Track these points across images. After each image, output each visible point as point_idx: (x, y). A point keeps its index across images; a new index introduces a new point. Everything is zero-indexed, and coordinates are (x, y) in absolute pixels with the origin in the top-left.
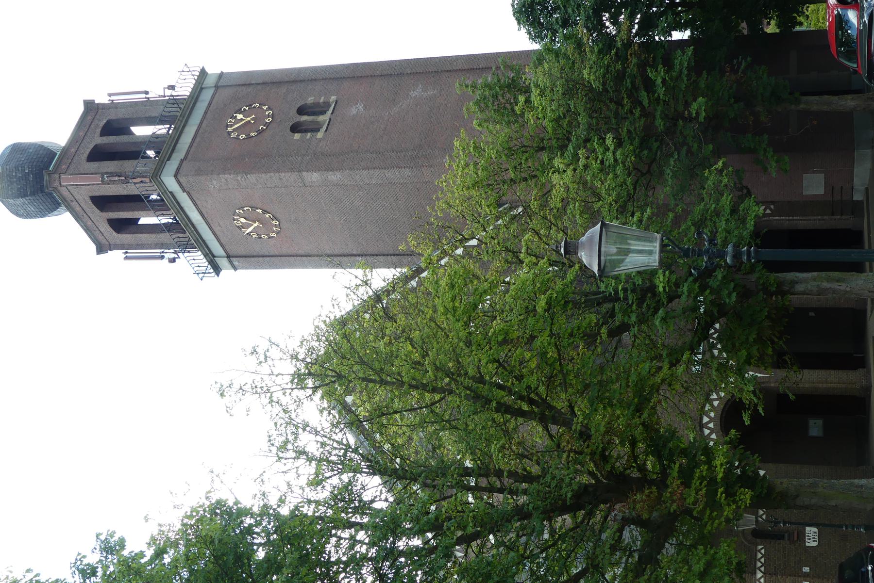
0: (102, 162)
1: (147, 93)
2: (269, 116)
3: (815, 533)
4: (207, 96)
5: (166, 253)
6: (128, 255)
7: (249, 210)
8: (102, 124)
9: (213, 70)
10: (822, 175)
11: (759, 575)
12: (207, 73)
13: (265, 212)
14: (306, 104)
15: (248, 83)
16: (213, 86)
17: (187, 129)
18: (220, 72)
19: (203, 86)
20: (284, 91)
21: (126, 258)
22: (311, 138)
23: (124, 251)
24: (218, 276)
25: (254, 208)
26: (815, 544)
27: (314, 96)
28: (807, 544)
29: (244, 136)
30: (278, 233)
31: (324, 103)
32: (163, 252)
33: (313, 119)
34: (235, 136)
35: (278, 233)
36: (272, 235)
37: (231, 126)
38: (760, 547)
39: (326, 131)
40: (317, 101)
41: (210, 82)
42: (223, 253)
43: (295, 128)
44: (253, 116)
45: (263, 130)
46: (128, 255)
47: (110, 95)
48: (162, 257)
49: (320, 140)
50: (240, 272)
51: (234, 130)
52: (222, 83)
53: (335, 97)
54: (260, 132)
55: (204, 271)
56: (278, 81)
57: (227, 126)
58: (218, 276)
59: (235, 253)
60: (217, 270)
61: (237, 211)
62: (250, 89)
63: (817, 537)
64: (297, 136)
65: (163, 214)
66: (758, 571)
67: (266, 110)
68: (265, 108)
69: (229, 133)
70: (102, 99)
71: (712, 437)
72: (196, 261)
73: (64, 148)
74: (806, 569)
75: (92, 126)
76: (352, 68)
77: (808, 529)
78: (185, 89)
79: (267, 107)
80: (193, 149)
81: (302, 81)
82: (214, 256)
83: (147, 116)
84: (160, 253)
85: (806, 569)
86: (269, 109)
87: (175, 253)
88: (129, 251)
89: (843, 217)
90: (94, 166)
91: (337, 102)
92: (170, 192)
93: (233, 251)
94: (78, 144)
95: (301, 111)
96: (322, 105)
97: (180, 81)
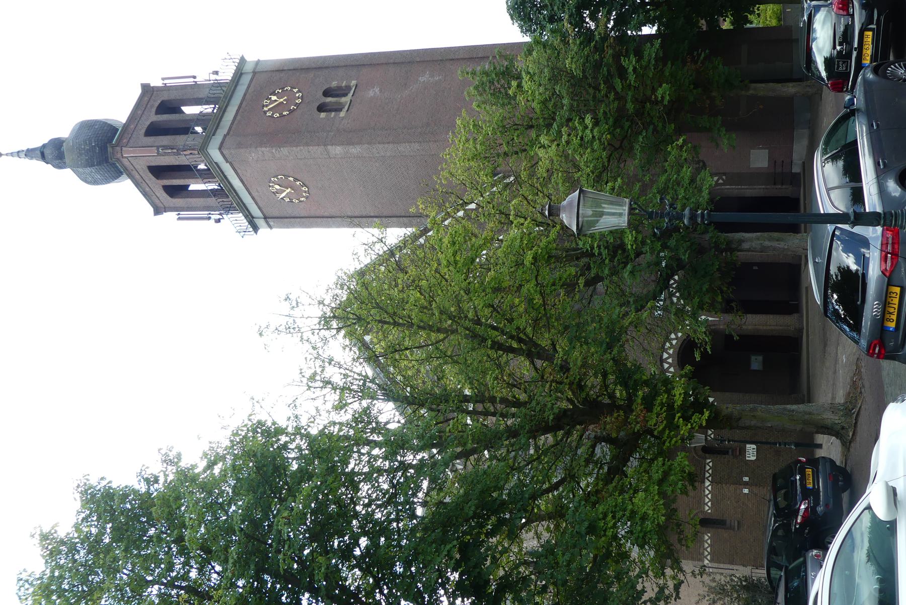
0: (157, 137)
1: (194, 77)
3: (754, 449)
4: (246, 80)
8: (157, 104)
9: (251, 58)
10: (767, 151)
11: (707, 483)
12: (246, 61)
13: (296, 180)
17: (229, 108)
18: (257, 60)
19: (243, 72)
21: (179, 219)
23: (177, 213)
25: (287, 176)
26: (754, 458)
27: (338, 80)
28: (747, 459)
30: (307, 198)
31: (346, 86)
32: (210, 214)
34: (270, 114)
35: (307, 198)
37: (267, 106)
38: (708, 461)
39: (348, 110)
41: (248, 68)
42: (260, 215)
43: (321, 108)
44: (286, 98)
45: (294, 110)
47: (163, 79)
50: (274, 230)
51: (269, 110)
52: (259, 69)
54: (291, 111)
57: (264, 106)
59: (271, 215)
60: (255, 228)
61: (272, 179)
63: (755, 453)
64: (323, 115)
66: (706, 480)
67: (297, 93)
68: (295, 90)
69: (265, 112)
70: (157, 82)
71: (670, 370)
73: (125, 124)
74: (746, 479)
75: (149, 106)
77: (748, 446)
78: (227, 75)
80: (234, 126)
81: (327, 68)
82: (253, 217)
84: (208, 214)
85: (746, 479)
86: (299, 91)
87: (220, 214)
88: (181, 213)
89: (784, 187)
90: (151, 140)
91: (356, 85)
92: (216, 163)
93: (270, 212)
94: (137, 121)
95: (327, 93)
96: (344, 88)
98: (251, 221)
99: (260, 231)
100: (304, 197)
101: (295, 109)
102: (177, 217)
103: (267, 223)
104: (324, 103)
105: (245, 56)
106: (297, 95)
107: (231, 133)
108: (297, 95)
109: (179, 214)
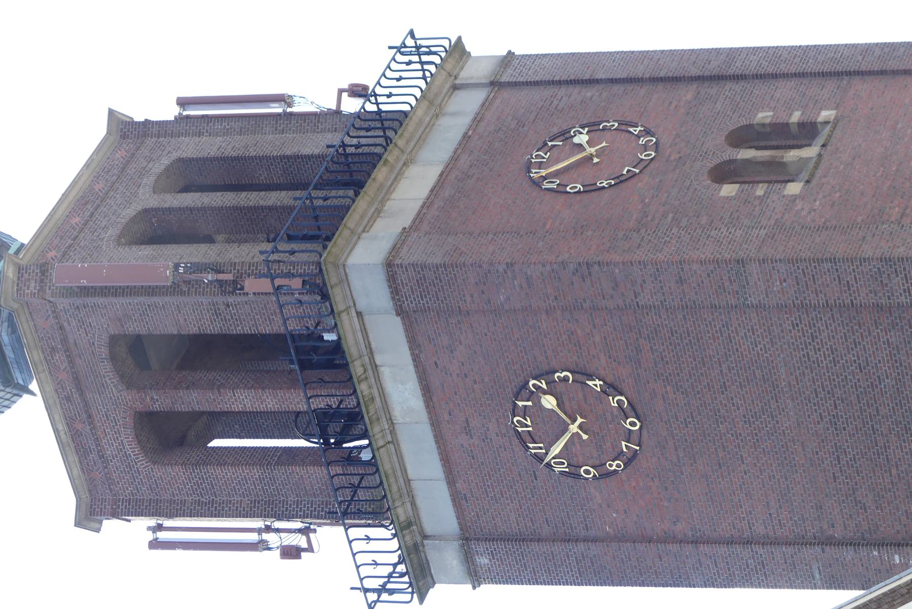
2: (645, 147)
5: (278, 530)
6: (163, 535)
7: (566, 379)
14: (751, 126)
15: (587, 77)
16: (488, 81)
18: (504, 53)
20: (689, 96)
21: (155, 544)
22: (767, 194)
23: (152, 522)
24: (421, 600)
25: (583, 374)
27: (774, 109)
29: (579, 186)
30: (630, 460)
31: (801, 125)
32: (268, 529)
33: (772, 156)
35: (630, 460)
36: (614, 466)
37: (540, 165)
40: (780, 120)
46: (163, 535)
47: (183, 103)
48: (260, 546)
49: (794, 198)
50: (488, 590)
53: (834, 112)
55: (385, 597)
56: (671, 75)
58: (421, 600)
61: (532, 382)
62: (590, 92)
64: (728, 190)
65: (322, 380)
72: (373, 546)
76: (878, 52)
79: (639, 128)
83: (289, 153)
84: (259, 531)
87: (305, 531)
88: (168, 523)
96: (794, 130)
97: (384, 82)
98: (416, 546)
99: (438, 593)
100: (619, 455)
101: (635, 174)
102: (150, 536)
103: (468, 559)
104: (731, 162)
105: (463, 40)
106: (642, 141)
107: (425, 227)
108: (642, 141)
109: (160, 528)
